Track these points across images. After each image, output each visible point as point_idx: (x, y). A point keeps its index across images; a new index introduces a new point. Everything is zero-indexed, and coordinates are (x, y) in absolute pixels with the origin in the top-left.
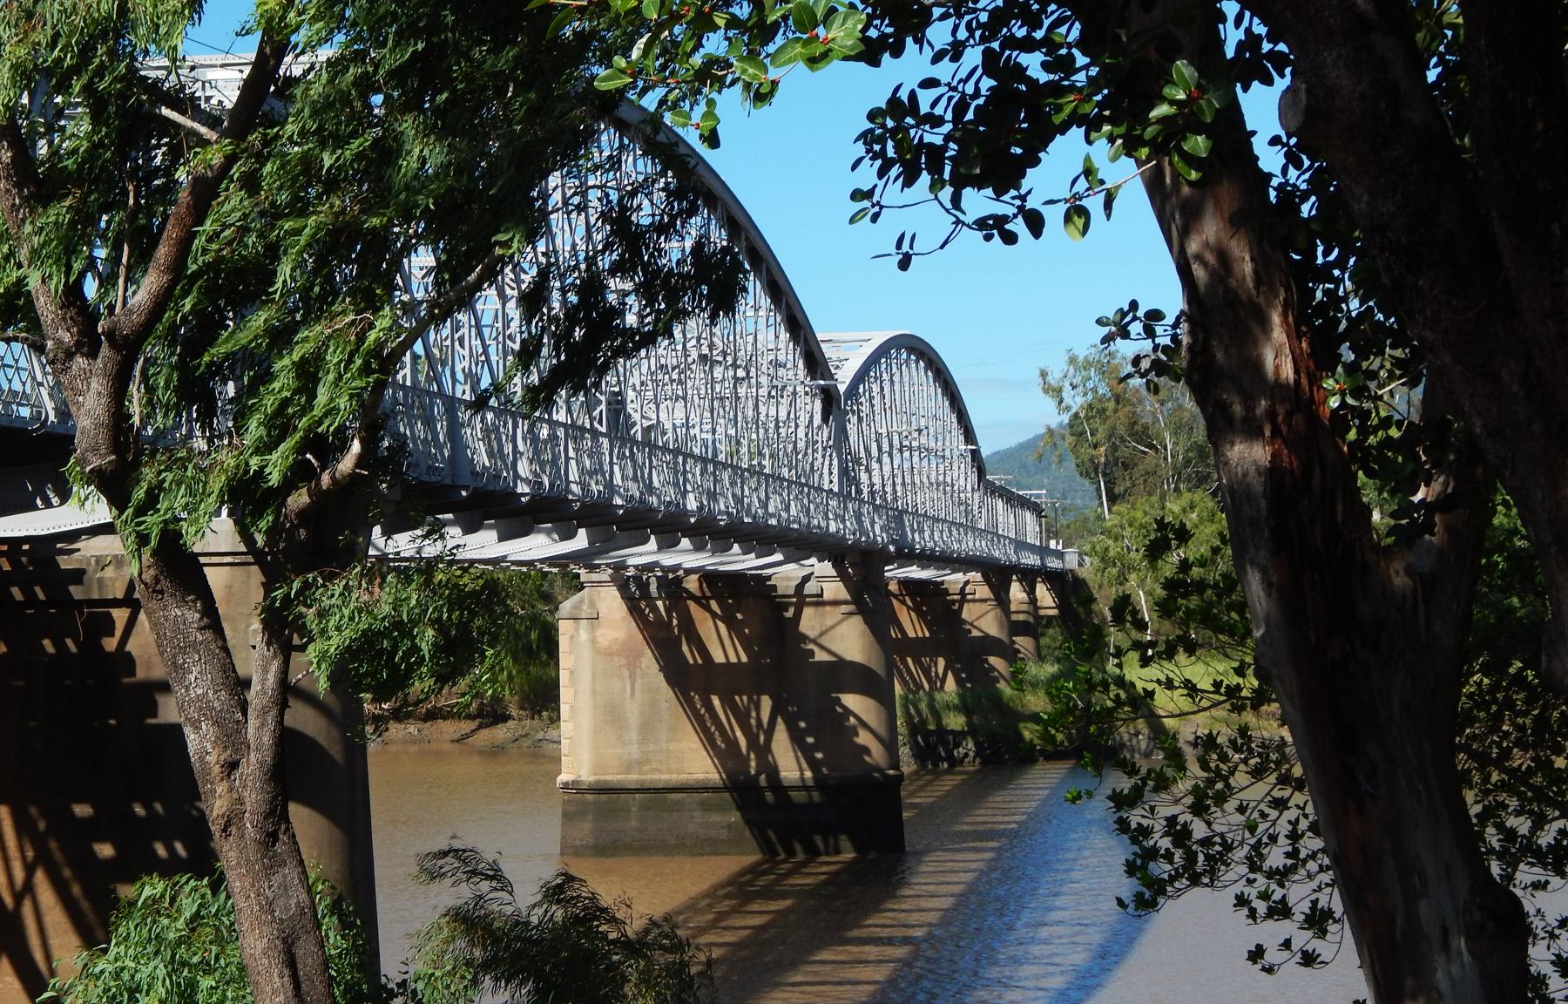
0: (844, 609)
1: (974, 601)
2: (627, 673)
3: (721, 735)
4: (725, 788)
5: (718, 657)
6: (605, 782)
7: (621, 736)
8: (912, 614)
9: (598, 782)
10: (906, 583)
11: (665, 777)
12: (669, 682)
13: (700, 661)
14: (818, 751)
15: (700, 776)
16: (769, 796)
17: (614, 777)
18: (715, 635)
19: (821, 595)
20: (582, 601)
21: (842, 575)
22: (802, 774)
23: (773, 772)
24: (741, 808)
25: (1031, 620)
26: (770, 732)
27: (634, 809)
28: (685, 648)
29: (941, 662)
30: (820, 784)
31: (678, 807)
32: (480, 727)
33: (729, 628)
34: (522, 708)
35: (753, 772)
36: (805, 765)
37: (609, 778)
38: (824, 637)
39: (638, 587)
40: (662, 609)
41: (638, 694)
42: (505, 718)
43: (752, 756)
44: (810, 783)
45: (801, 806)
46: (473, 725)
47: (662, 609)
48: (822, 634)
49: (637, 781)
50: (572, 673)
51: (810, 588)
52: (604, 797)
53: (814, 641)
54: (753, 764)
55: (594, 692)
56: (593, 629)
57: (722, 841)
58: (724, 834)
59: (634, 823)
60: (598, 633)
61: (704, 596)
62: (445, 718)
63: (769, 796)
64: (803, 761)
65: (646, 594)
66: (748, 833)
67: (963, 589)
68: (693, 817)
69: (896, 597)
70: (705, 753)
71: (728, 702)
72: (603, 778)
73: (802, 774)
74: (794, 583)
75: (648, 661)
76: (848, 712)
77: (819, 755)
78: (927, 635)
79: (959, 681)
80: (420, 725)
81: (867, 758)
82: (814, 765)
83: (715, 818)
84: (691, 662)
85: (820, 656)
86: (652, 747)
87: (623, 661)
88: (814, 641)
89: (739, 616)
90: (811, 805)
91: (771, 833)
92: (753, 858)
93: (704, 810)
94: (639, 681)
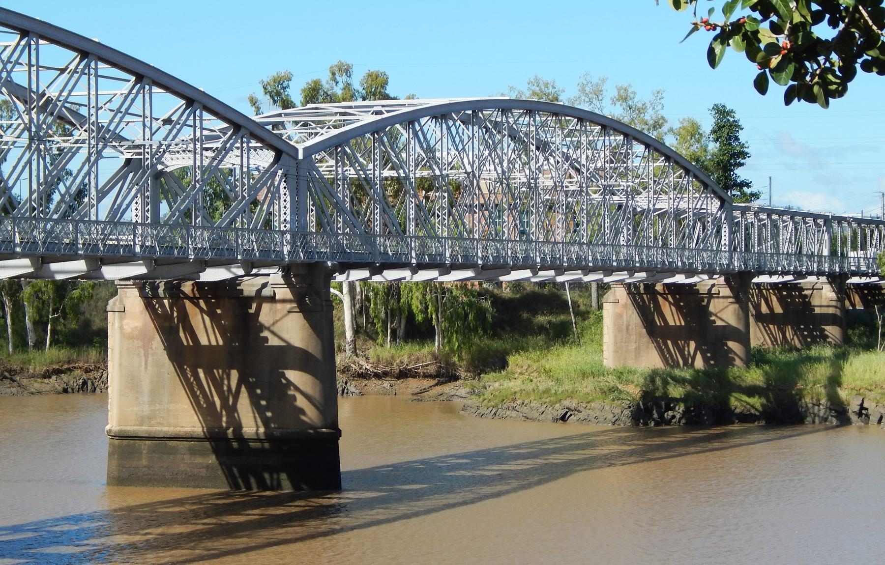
0: (288, 306)
1: (718, 297)
2: (142, 353)
3: (203, 398)
4: (205, 438)
5: (204, 341)
6: (125, 431)
7: (137, 398)
8: (673, 308)
9: (120, 431)
10: (857, 286)
11: (165, 429)
12: (170, 359)
13: (191, 344)
14: (268, 411)
15: (188, 429)
16: (235, 445)
17: (132, 428)
18: (202, 326)
19: (719, 294)
20: (117, 300)
21: (288, 283)
22: (257, 430)
23: (238, 427)
24: (216, 452)
25: (838, 313)
26: (236, 396)
27: (145, 452)
28: (182, 334)
29: (693, 345)
30: (269, 437)
31: (174, 451)
32: (437, 384)
33: (212, 320)
34: (468, 371)
35: (224, 424)
36: (260, 423)
37: (128, 428)
38: (279, 324)
39: (151, 290)
40: (167, 305)
41: (149, 368)
42: (456, 378)
43: (224, 413)
44: (262, 437)
45: (256, 451)
46: (432, 382)
47: (167, 305)
48: (274, 324)
49: (146, 432)
50: (112, 350)
51: (266, 292)
52: (125, 442)
53: (268, 329)
54: (224, 419)
55: (120, 365)
56: (121, 319)
57: (202, 477)
58: (203, 472)
59: (144, 462)
60: (125, 322)
61: (195, 297)
62: (414, 377)
63: (235, 445)
64: (259, 420)
65: (156, 296)
66: (220, 472)
67: (710, 290)
68: (183, 459)
69: (661, 295)
70: (193, 412)
71: (209, 374)
72: (124, 428)
73: (257, 430)
74: (256, 289)
75: (157, 344)
76: (289, 383)
77: (269, 414)
78: (683, 324)
79: (706, 360)
80: (394, 382)
81: (303, 418)
82: (266, 422)
83: (199, 460)
84: (185, 344)
85: (273, 341)
86: (158, 406)
87: (140, 343)
88: (268, 329)
89: (219, 311)
90: (263, 450)
91: (235, 470)
92: (225, 489)
93: (191, 454)
94: (150, 358)
